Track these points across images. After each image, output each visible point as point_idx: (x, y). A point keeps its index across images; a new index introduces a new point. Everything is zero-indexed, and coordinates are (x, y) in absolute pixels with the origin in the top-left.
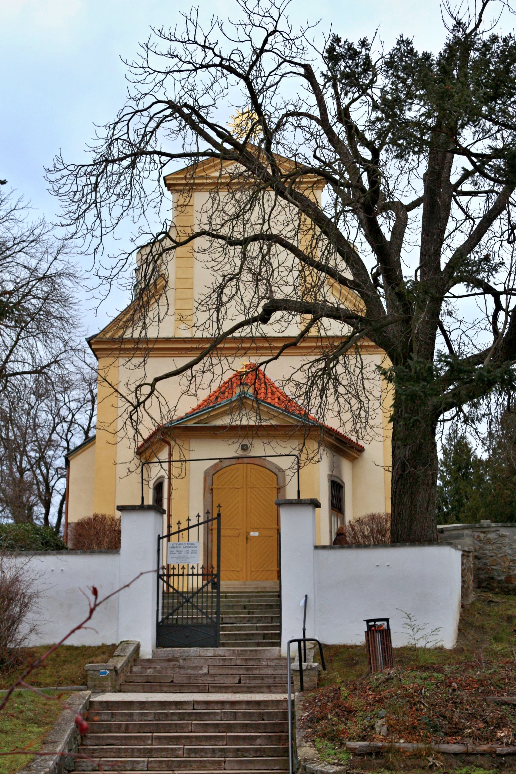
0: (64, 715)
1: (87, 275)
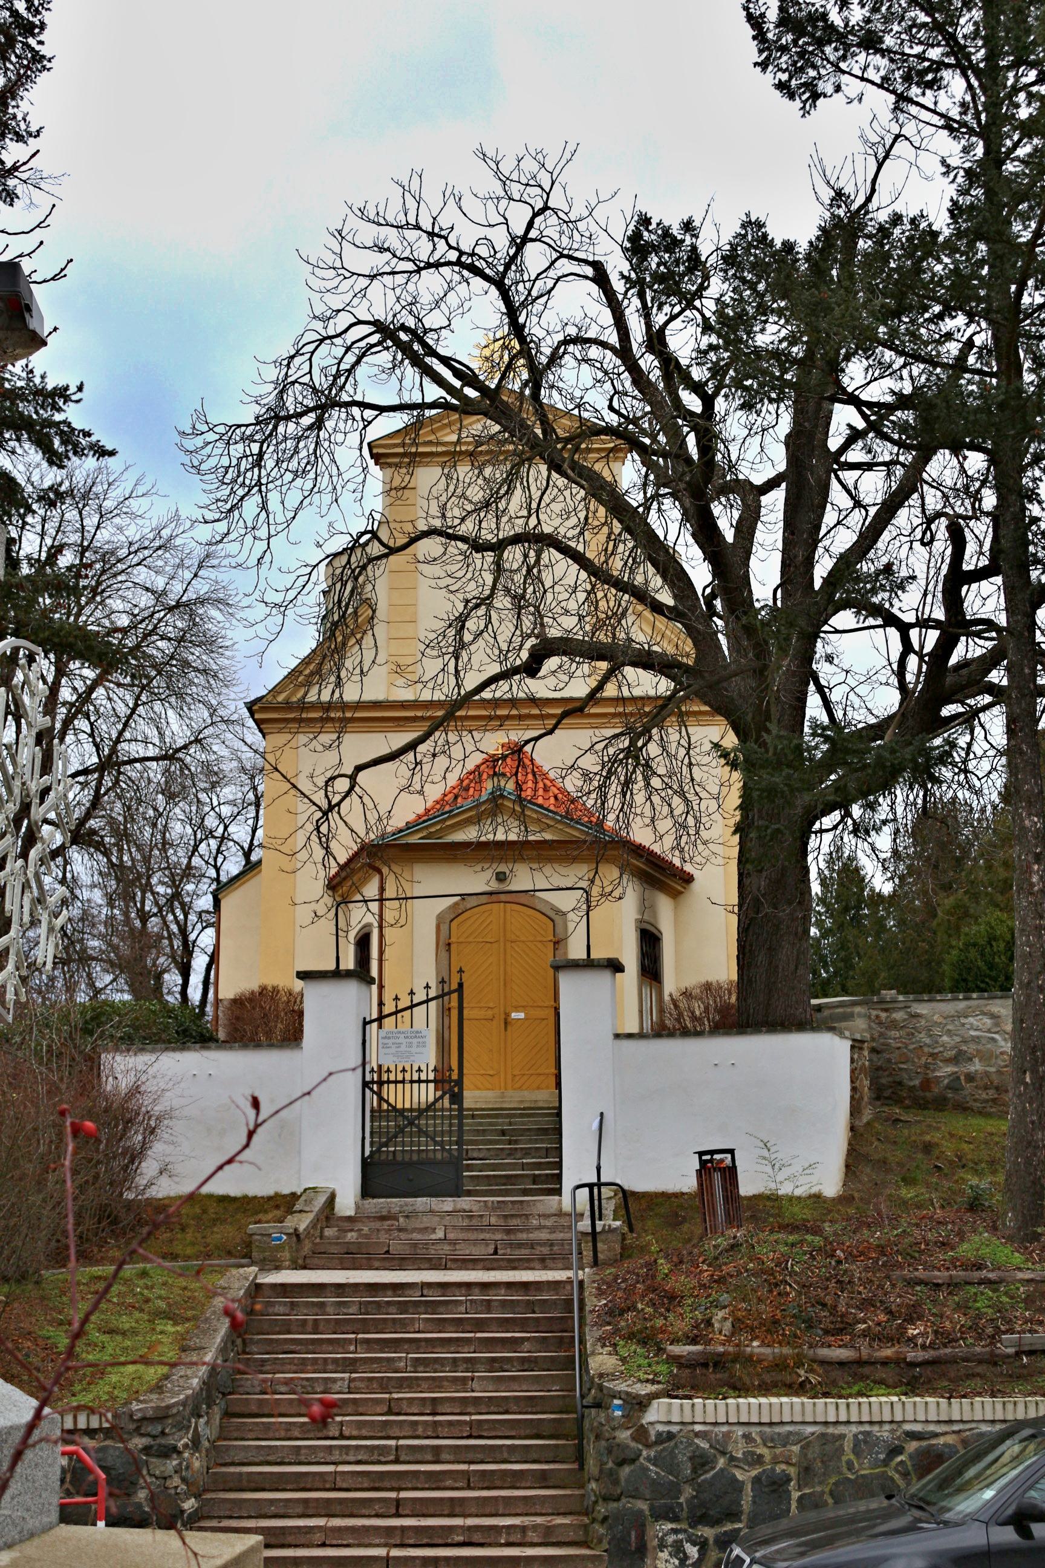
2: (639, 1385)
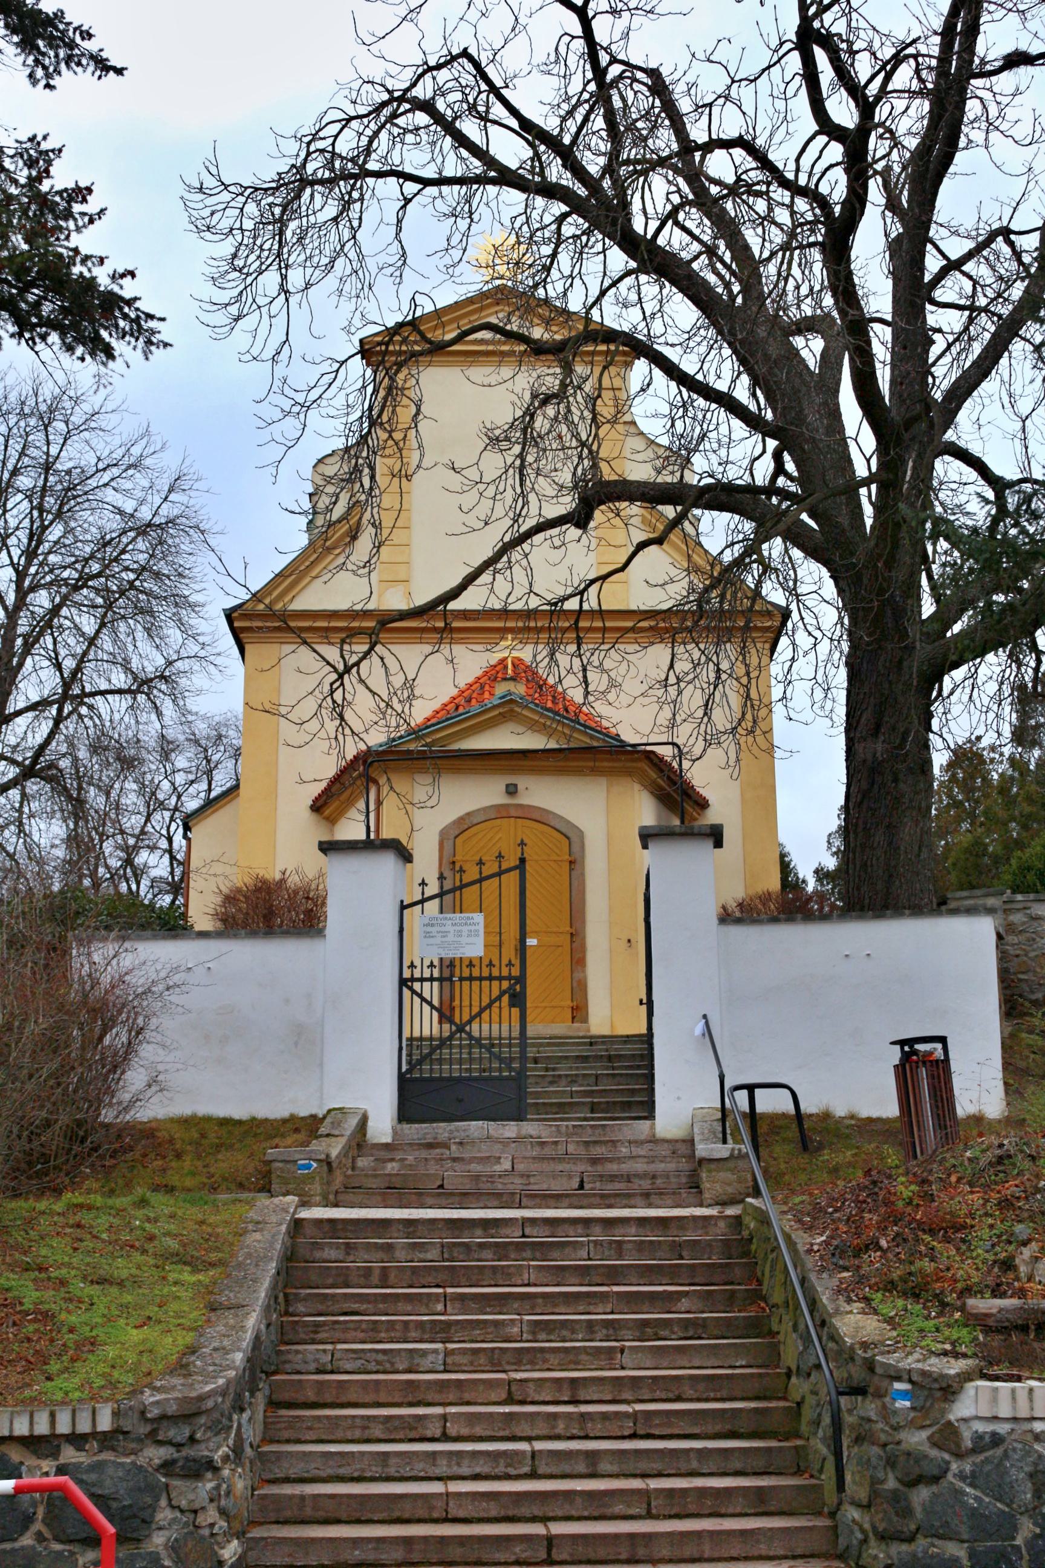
0: (248, 1247)
2: (933, 1360)
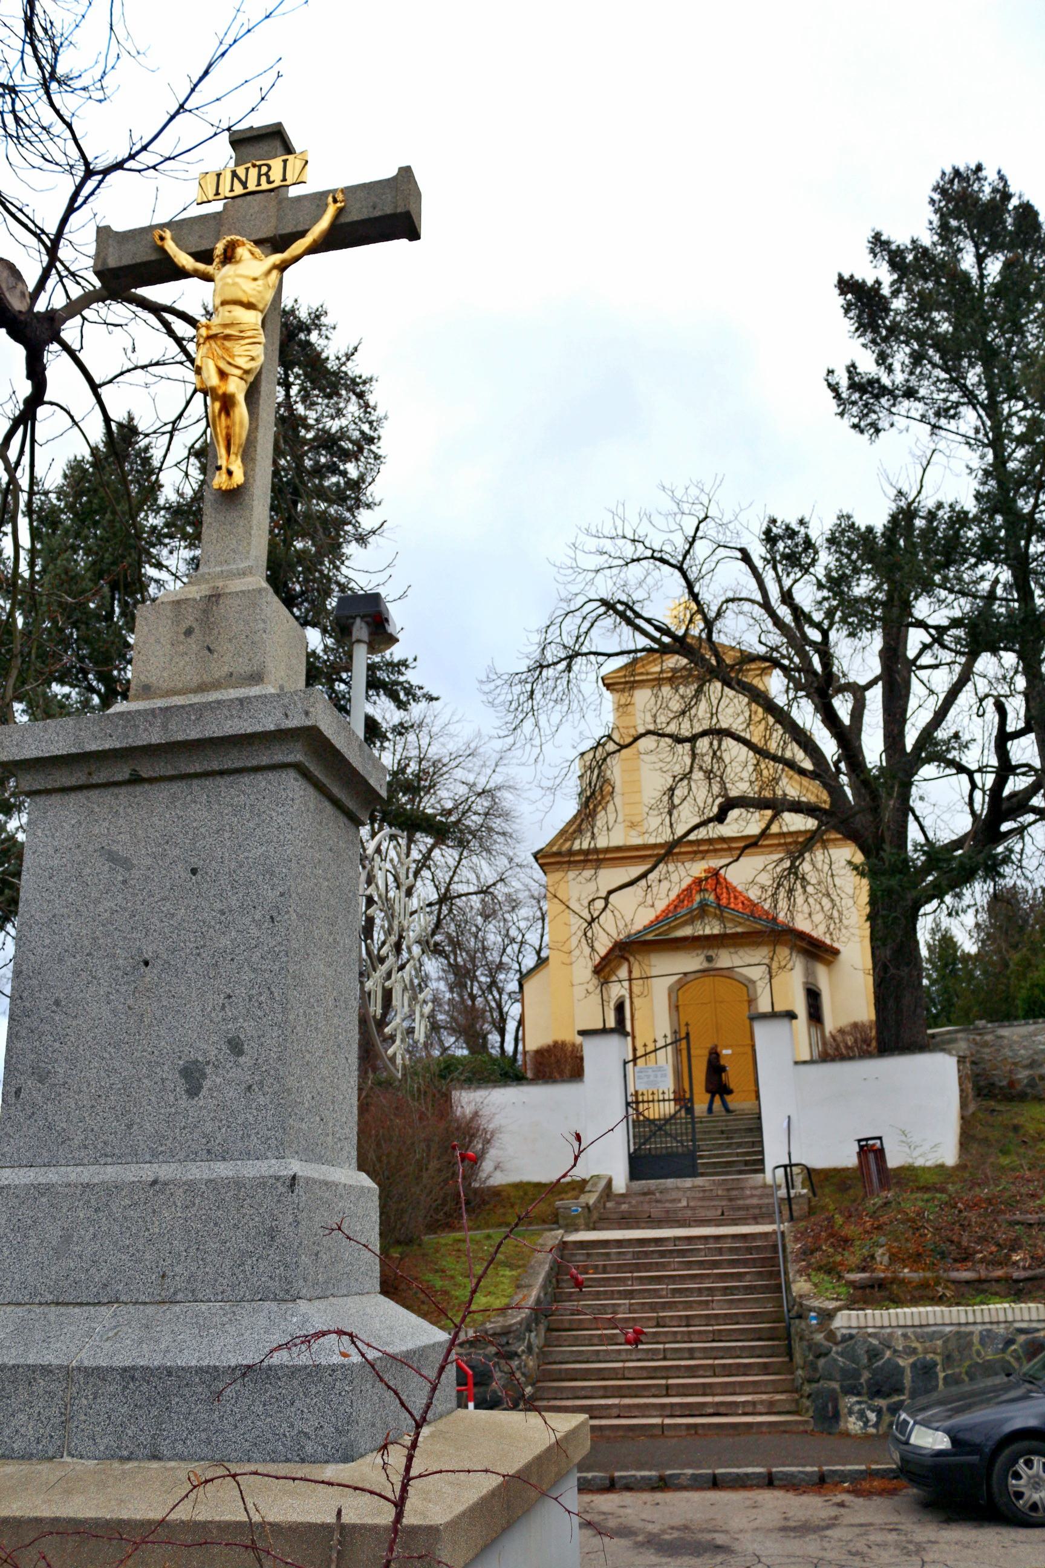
1: (527, 786)
